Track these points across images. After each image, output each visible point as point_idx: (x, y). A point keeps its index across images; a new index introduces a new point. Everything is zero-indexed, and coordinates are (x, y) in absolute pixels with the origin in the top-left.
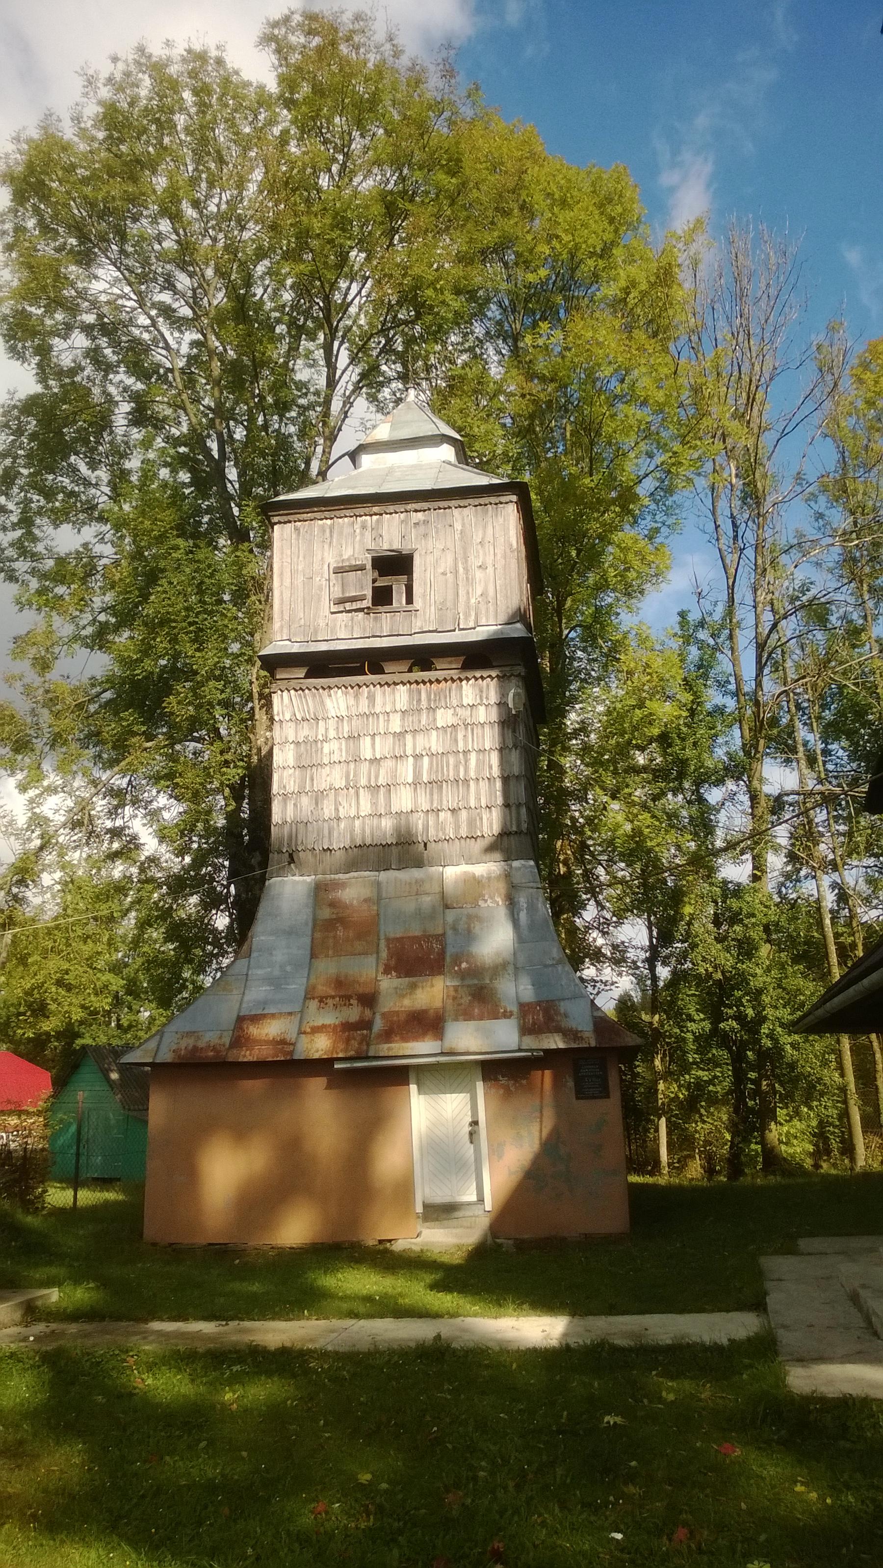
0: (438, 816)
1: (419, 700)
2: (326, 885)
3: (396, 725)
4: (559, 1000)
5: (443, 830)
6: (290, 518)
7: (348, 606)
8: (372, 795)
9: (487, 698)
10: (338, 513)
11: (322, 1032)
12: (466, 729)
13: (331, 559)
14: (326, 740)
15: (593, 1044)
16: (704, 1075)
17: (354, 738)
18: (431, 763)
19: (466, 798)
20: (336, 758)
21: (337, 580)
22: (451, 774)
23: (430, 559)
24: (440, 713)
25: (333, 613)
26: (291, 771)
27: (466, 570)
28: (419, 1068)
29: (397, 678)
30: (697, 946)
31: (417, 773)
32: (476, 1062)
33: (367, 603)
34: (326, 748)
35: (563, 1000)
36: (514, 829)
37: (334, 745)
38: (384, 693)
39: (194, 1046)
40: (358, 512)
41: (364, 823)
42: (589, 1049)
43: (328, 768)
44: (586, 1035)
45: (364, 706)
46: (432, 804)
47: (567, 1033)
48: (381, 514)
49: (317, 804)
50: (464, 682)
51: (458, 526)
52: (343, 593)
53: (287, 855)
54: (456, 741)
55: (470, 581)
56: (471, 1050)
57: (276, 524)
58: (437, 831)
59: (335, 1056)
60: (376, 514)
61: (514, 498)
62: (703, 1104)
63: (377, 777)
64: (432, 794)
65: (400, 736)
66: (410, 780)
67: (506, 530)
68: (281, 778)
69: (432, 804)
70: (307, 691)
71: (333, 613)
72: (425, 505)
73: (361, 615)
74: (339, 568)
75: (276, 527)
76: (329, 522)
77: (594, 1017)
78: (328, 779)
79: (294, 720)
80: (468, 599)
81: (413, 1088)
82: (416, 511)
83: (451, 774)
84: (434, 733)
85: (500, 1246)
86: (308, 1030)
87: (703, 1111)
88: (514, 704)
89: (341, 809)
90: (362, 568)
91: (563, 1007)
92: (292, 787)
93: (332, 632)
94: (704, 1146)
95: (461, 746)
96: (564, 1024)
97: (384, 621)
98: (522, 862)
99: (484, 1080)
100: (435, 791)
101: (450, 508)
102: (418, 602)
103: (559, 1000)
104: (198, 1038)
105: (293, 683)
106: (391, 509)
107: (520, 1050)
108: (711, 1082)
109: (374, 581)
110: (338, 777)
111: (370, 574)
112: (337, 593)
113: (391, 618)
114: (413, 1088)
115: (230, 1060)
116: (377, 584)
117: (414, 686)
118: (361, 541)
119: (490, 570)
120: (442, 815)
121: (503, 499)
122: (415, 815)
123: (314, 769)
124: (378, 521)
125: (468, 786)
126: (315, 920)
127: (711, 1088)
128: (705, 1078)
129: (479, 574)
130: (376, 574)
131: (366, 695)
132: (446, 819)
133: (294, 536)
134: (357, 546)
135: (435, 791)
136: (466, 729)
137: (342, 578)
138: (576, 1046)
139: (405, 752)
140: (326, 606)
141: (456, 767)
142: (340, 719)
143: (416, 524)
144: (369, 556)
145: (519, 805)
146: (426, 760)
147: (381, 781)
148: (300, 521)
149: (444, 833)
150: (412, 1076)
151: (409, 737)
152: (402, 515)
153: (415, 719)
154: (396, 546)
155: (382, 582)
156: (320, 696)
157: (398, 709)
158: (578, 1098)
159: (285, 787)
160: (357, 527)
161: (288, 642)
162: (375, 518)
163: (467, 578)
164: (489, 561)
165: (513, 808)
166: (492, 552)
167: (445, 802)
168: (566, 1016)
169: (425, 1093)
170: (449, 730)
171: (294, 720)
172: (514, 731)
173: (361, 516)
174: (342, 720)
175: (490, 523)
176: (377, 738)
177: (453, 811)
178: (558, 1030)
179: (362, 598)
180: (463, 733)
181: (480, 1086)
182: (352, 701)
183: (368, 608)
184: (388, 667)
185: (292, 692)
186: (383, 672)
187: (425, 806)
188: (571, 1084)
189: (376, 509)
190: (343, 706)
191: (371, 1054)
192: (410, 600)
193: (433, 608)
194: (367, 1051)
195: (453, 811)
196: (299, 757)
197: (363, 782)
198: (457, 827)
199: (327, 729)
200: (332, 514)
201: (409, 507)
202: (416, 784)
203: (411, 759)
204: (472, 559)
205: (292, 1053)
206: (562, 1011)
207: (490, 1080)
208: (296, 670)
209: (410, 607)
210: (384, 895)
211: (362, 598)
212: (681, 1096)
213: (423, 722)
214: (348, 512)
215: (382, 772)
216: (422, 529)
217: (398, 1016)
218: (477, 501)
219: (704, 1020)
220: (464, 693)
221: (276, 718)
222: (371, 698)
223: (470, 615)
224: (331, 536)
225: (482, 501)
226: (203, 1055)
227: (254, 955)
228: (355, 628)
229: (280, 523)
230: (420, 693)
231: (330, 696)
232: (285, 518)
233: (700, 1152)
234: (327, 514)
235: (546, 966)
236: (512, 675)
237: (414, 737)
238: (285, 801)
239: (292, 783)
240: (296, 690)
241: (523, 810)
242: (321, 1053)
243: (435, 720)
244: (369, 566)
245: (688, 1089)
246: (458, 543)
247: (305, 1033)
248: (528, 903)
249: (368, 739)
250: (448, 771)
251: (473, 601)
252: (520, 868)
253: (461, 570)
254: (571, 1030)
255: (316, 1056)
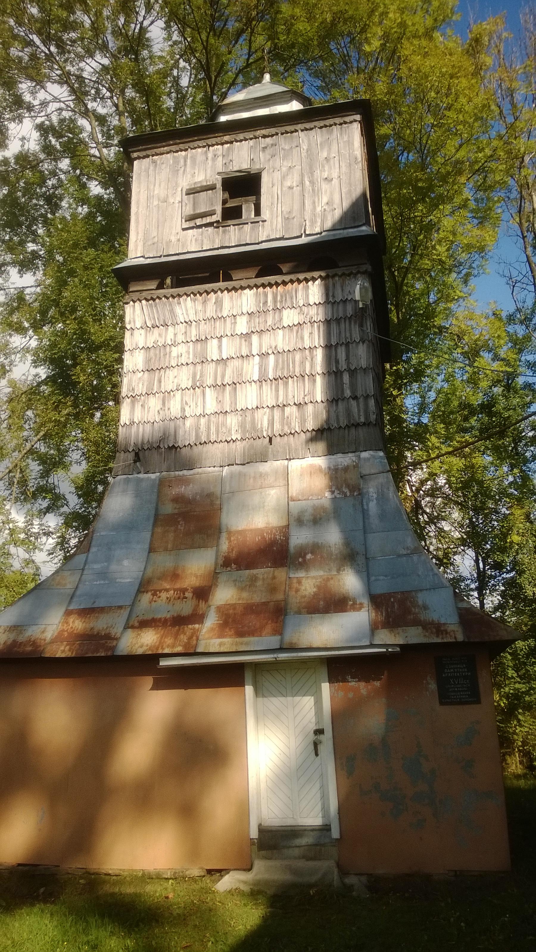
0: (283, 411)
1: (265, 303)
2: (170, 481)
3: (242, 326)
4: (416, 591)
5: (289, 425)
6: (149, 152)
7: (199, 222)
8: (218, 393)
9: (333, 296)
10: (191, 145)
11: (151, 627)
12: (312, 326)
13: (185, 183)
14: (174, 344)
15: (460, 637)
16: (523, 687)
17: (201, 341)
18: (277, 362)
19: (312, 392)
20: (183, 360)
21: (189, 201)
22: (297, 370)
23: (277, 175)
24: (285, 313)
25: (184, 229)
26: (140, 375)
27: (312, 182)
28: (256, 666)
29: (244, 283)
30: (524, 572)
31: (263, 369)
32: (321, 659)
33: (217, 217)
34: (175, 351)
35: (421, 590)
36: (362, 420)
37: (182, 349)
38: (231, 298)
39: (14, 641)
40: (210, 141)
41: (209, 421)
42: (455, 645)
43: (175, 370)
44: (451, 628)
45: (211, 310)
46: (277, 398)
47: (427, 626)
48: (231, 142)
49: (164, 404)
50: (310, 283)
51: (305, 147)
52: (194, 210)
53: (133, 454)
54: (302, 338)
55: (315, 192)
56: (315, 646)
57: (136, 159)
58: (283, 425)
59: (160, 651)
60: (227, 143)
61: (358, 117)
62: (520, 711)
63: (223, 376)
64: (277, 391)
65: (247, 336)
66: (256, 378)
67: (350, 143)
68: (130, 381)
69: (277, 398)
70: (157, 301)
71: (184, 229)
72: (273, 131)
73: (210, 229)
74: (190, 189)
75: (136, 163)
76: (183, 153)
77: (459, 609)
78: (176, 381)
79: (145, 326)
80: (314, 208)
81: (249, 690)
82: (264, 137)
83: (297, 370)
84: (280, 332)
85: (350, 888)
86: (137, 624)
87: (520, 717)
88: (361, 296)
89: (187, 408)
90: (212, 188)
91: (421, 598)
92: (140, 389)
93: (183, 246)
94: (523, 746)
95: (307, 344)
96: (423, 616)
97: (232, 234)
98: (371, 452)
99: (330, 681)
100: (281, 387)
101: (296, 131)
102: (265, 213)
103: (416, 591)
104: (21, 632)
105: (144, 294)
106: (241, 136)
107: (372, 646)
108: (527, 693)
109: (224, 202)
110: (185, 378)
111: (219, 195)
112: (189, 211)
113: (239, 229)
114: (249, 690)
115: (47, 655)
116: (227, 205)
117: (261, 289)
118: (214, 166)
119: (335, 182)
120: (287, 410)
121: (347, 119)
122: (260, 411)
123: (162, 371)
124: (228, 149)
125: (315, 381)
126: (156, 515)
127: (527, 698)
128: (524, 690)
129: (325, 186)
130: (227, 195)
131: (214, 301)
132: (291, 414)
133: (152, 168)
134: (209, 171)
135: (281, 387)
136: (312, 326)
137: (194, 198)
138: (439, 640)
139: (251, 351)
140: (178, 223)
141: (302, 363)
142: (188, 323)
143: (264, 148)
144: (220, 178)
145: (367, 397)
146: (272, 358)
147: (227, 380)
148: (157, 154)
149: (289, 427)
150: (248, 676)
151: (255, 338)
152: (252, 142)
153: (262, 320)
154: (245, 166)
155: (231, 204)
156: (170, 305)
157: (245, 311)
158: (442, 703)
159: (133, 389)
160: (210, 155)
161: (142, 259)
162: (226, 146)
163: (313, 190)
164: (335, 174)
165: (361, 400)
166: (337, 166)
167: (290, 396)
168: (425, 607)
169: (264, 696)
170: (295, 329)
171: (145, 326)
172: (361, 326)
173: (213, 145)
174: (190, 326)
175: (335, 142)
176: (224, 340)
177: (299, 405)
178: (417, 623)
179: (212, 213)
180: (309, 330)
181: (326, 687)
182: (199, 307)
183: (218, 222)
184: (235, 275)
185: (144, 302)
186: (232, 280)
187: (271, 402)
188: (433, 686)
189: (227, 138)
190: (191, 312)
191: (199, 650)
192: (258, 212)
193: (280, 219)
194: (196, 646)
195: (299, 405)
196: (148, 361)
197: (209, 381)
198: (303, 421)
199: (175, 335)
200: (186, 146)
201: (259, 133)
202: (261, 381)
203: (257, 359)
204: (317, 173)
205: (114, 648)
206: (420, 603)
207: (338, 681)
208: (148, 283)
209: (257, 219)
210: (228, 489)
211: (212, 213)
212: (502, 705)
213: (270, 322)
214: (201, 143)
215: (229, 372)
216: (269, 151)
217: (234, 609)
218: (322, 123)
219: (464, 668)
220: (310, 291)
221: (128, 326)
222: (219, 304)
223: (316, 222)
224: (185, 165)
225: (327, 122)
226: (21, 650)
227: (93, 550)
228: (205, 241)
229: (139, 158)
230: (266, 295)
231: (179, 303)
232: (144, 153)
233: (519, 750)
234: (182, 146)
235: (399, 556)
236: (359, 272)
237: (260, 337)
238: (133, 404)
239: (141, 385)
240: (147, 300)
241: (372, 402)
242: (145, 648)
243: (281, 319)
244: (219, 186)
245: (507, 699)
246: (304, 160)
247: (133, 627)
248: (378, 493)
249: (215, 342)
250: (294, 367)
251: (319, 209)
252: (368, 459)
253: (307, 183)
254: (432, 623)
255: (140, 651)
